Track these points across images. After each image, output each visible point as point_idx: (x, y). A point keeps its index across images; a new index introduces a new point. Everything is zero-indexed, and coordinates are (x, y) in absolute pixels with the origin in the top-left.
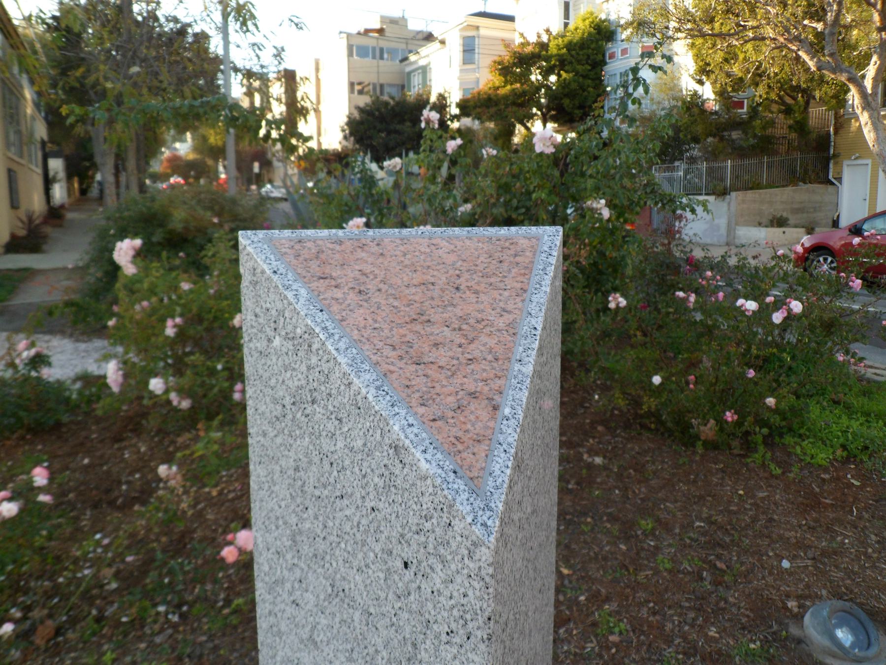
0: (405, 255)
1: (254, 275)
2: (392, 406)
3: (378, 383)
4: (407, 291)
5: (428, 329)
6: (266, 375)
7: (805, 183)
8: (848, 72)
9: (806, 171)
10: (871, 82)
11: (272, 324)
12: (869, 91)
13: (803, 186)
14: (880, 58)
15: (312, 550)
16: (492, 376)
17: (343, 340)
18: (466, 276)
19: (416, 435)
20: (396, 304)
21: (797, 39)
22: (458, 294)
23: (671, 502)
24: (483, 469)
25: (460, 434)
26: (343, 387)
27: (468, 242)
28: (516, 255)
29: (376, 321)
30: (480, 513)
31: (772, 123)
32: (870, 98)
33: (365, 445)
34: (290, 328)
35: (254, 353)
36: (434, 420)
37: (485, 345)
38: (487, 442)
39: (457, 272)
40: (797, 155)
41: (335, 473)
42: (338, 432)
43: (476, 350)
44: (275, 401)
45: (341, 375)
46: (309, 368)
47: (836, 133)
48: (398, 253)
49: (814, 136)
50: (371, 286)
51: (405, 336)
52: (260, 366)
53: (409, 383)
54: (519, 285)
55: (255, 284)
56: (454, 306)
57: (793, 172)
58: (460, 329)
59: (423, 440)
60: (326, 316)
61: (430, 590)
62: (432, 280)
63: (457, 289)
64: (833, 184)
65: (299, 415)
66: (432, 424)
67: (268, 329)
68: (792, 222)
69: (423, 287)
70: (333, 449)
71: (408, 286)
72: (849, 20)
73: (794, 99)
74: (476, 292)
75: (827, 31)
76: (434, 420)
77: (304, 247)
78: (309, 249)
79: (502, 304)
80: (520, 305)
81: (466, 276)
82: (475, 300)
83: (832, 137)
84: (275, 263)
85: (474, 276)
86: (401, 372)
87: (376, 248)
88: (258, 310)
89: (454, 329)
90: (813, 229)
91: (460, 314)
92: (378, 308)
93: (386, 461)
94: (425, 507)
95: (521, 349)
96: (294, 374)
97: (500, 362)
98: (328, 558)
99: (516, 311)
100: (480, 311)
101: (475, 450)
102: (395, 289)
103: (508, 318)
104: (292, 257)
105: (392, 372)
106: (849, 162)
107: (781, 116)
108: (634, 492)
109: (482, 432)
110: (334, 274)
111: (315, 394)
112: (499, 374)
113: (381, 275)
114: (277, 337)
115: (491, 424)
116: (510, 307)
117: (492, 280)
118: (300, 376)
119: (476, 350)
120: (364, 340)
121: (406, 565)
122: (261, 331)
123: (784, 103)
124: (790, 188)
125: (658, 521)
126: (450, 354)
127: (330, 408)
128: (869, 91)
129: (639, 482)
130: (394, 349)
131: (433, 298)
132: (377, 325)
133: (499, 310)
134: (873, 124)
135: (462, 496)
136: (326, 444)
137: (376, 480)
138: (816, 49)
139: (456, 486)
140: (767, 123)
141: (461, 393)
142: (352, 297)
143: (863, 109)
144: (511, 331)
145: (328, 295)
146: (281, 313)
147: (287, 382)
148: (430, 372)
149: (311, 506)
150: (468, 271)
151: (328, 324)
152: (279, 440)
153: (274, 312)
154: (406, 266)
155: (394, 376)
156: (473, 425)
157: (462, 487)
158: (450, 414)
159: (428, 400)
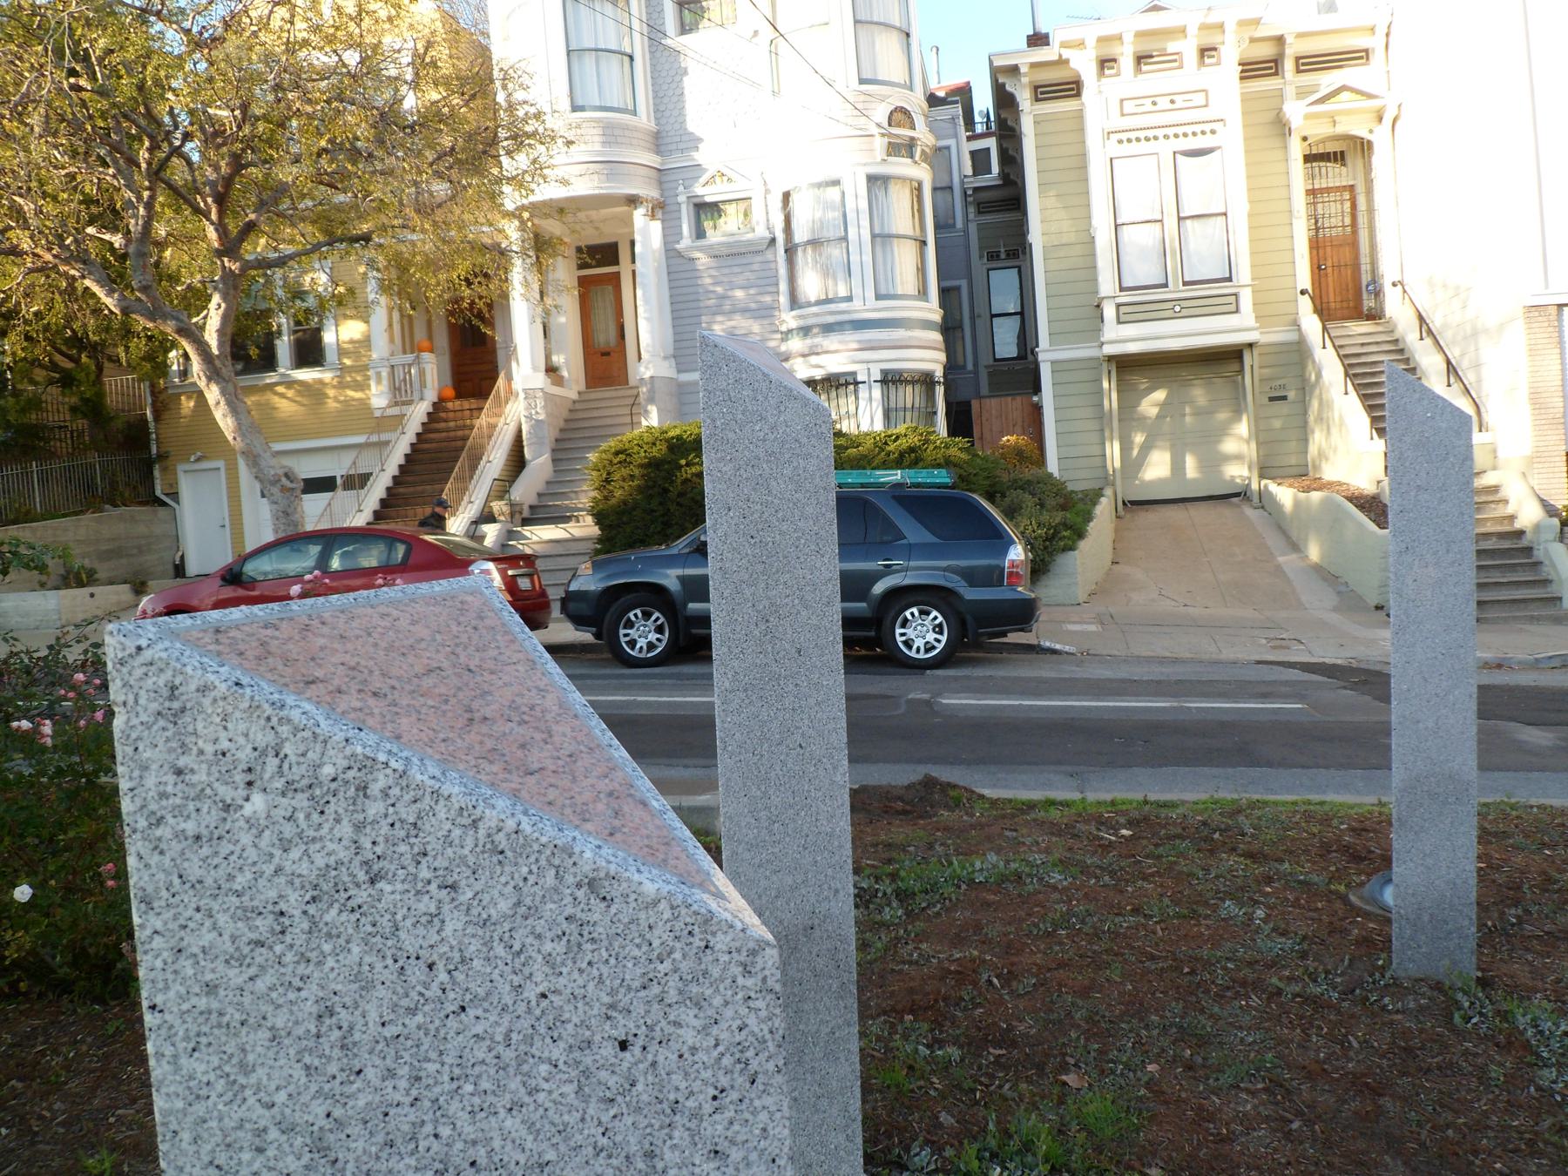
7: (115, 506)
8: (177, 319)
9: (113, 485)
10: (215, 336)
12: (215, 351)
13: (110, 511)
14: (225, 299)
21: (82, 258)
23: (125, 1106)
31: (35, 404)
32: (217, 363)
40: (93, 458)
47: (157, 418)
49: (119, 424)
57: (90, 487)
64: (164, 504)
68: (100, 575)
72: (163, 233)
73: (77, 361)
75: (131, 249)
83: (152, 425)
90: (143, 584)
106: (187, 467)
107: (54, 390)
108: (41, 1118)
121: (623, 1045)
123: (54, 366)
124: (89, 516)
125: (114, 1147)
128: (215, 351)
129: (44, 1096)
134: (229, 403)
138: (114, 279)
140: (29, 401)
143: (209, 379)
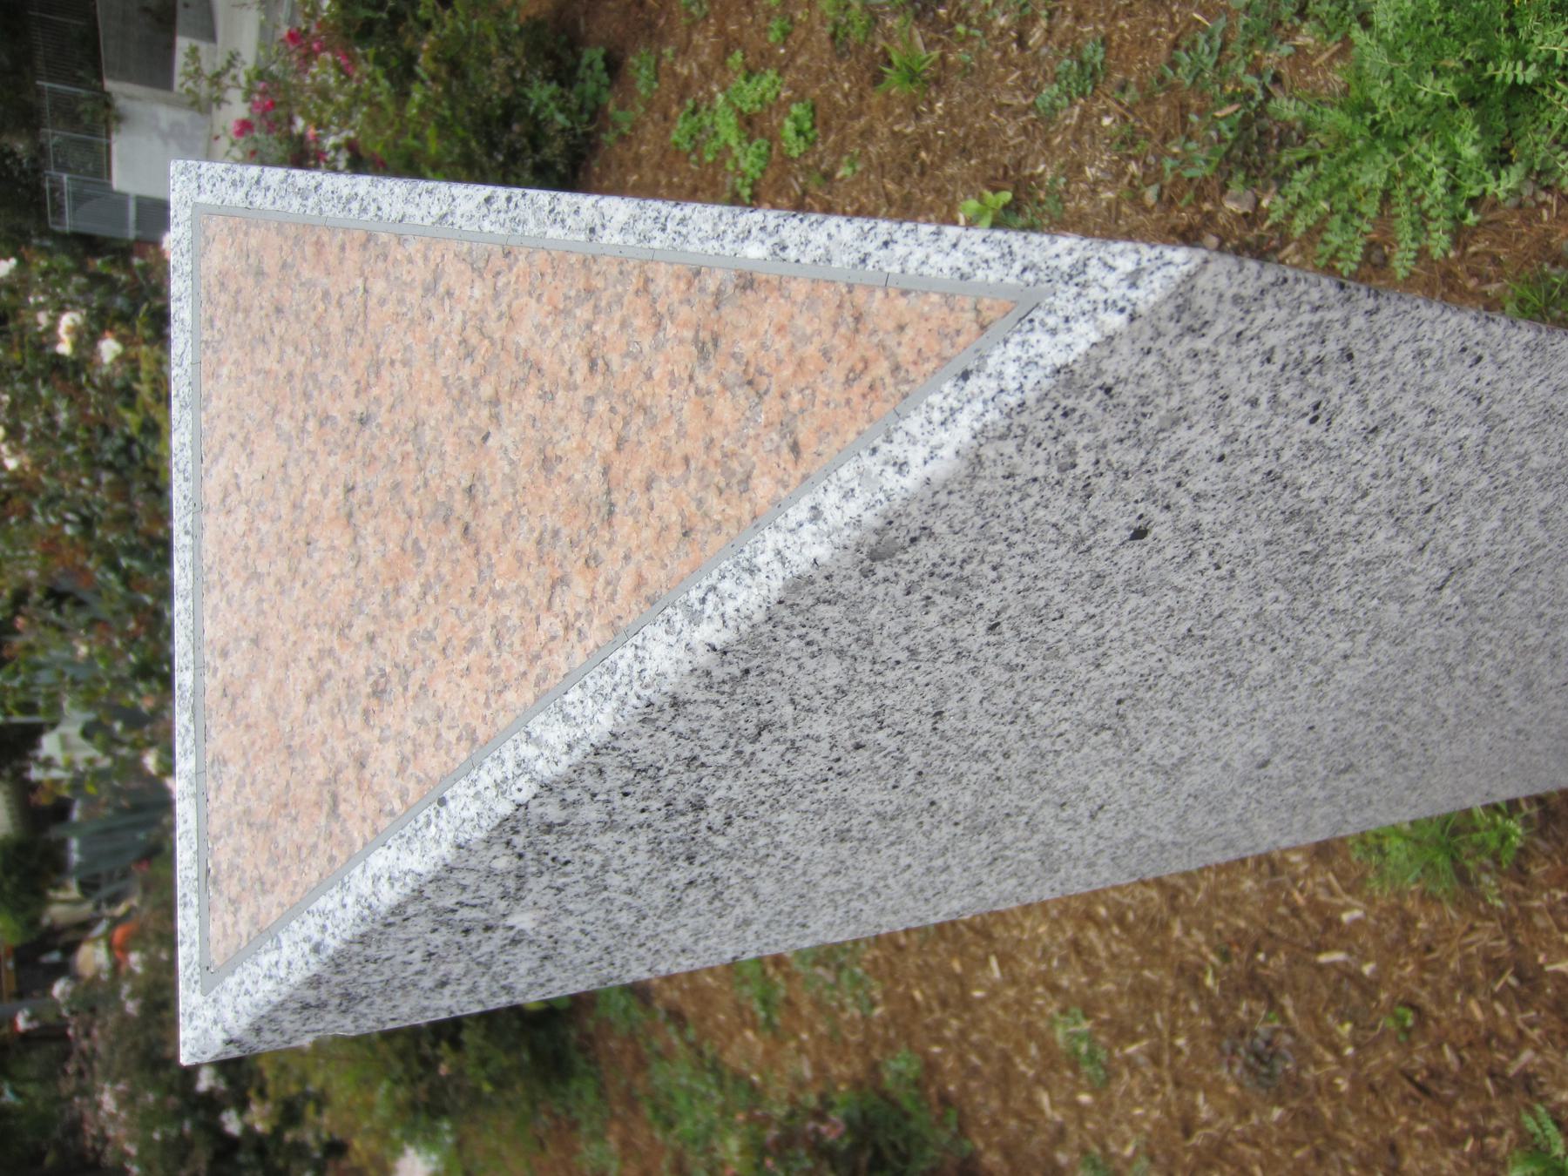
0: (256, 576)
1: (322, 1005)
2: (752, 571)
3: (679, 619)
4: (374, 560)
5: (495, 494)
6: (605, 938)
11: (473, 938)
15: (1017, 782)
16: (642, 302)
17: (537, 730)
18: (322, 400)
19: (849, 494)
20: (414, 589)
22: (382, 416)
24: (947, 297)
25: (837, 373)
26: (681, 725)
27: (216, 405)
28: (260, 273)
29: (473, 642)
30: (1094, 293)
33: (841, 653)
34: (490, 890)
35: (543, 976)
36: (795, 448)
37: (543, 330)
38: (860, 296)
39: (311, 425)
41: (881, 735)
42: (790, 734)
43: (562, 351)
44: (675, 905)
45: (647, 730)
46: (608, 826)
48: (250, 595)
50: (357, 663)
51: (519, 556)
52: (579, 958)
53: (676, 532)
54: (353, 256)
55: (348, 1000)
56: (419, 424)
58: (495, 402)
59: (862, 474)
60: (461, 788)
61: (1215, 466)
62: (337, 492)
63: (363, 421)
65: (721, 842)
66: (807, 455)
67: (485, 948)
69: (359, 517)
70: (825, 745)
71: (359, 560)
74: (376, 366)
76: (795, 448)
77: (233, 867)
78: (237, 851)
79: (412, 297)
80: (413, 247)
81: (322, 400)
82: (401, 372)
84: (287, 951)
85: (324, 378)
86: (638, 557)
87: (234, 658)
88: (427, 982)
89: (495, 418)
91: (445, 407)
92: (429, 637)
93: (897, 590)
94: (1040, 471)
95: (555, 232)
96: (616, 864)
97: (599, 283)
98: (1045, 744)
99: (434, 256)
100: (435, 349)
101: (890, 325)
102: (368, 594)
103: (454, 275)
104: (264, 901)
105: (641, 581)
109: (827, 313)
110: (321, 774)
111: (680, 804)
112: (635, 281)
113: (319, 637)
114: (510, 921)
115: (799, 290)
116: (421, 273)
117: (336, 327)
118: (624, 849)
119: (562, 351)
120: (538, 669)
122: (488, 966)
126: (575, 423)
127: (723, 759)
130: (563, 581)
131: (396, 486)
132: (487, 636)
133: (431, 303)
135: (1043, 348)
136: (811, 764)
137: (933, 618)
139: (1011, 370)
141: (701, 381)
142: (398, 716)
144: (498, 262)
145: (388, 786)
146: (442, 918)
147: (634, 882)
148: (637, 473)
149: (931, 794)
150: (307, 396)
151: (485, 779)
152: (767, 887)
153: (438, 939)
154: (294, 572)
155: (655, 575)
156: (807, 339)
157: (1013, 350)
158: (772, 404)
159: (729, 473)
